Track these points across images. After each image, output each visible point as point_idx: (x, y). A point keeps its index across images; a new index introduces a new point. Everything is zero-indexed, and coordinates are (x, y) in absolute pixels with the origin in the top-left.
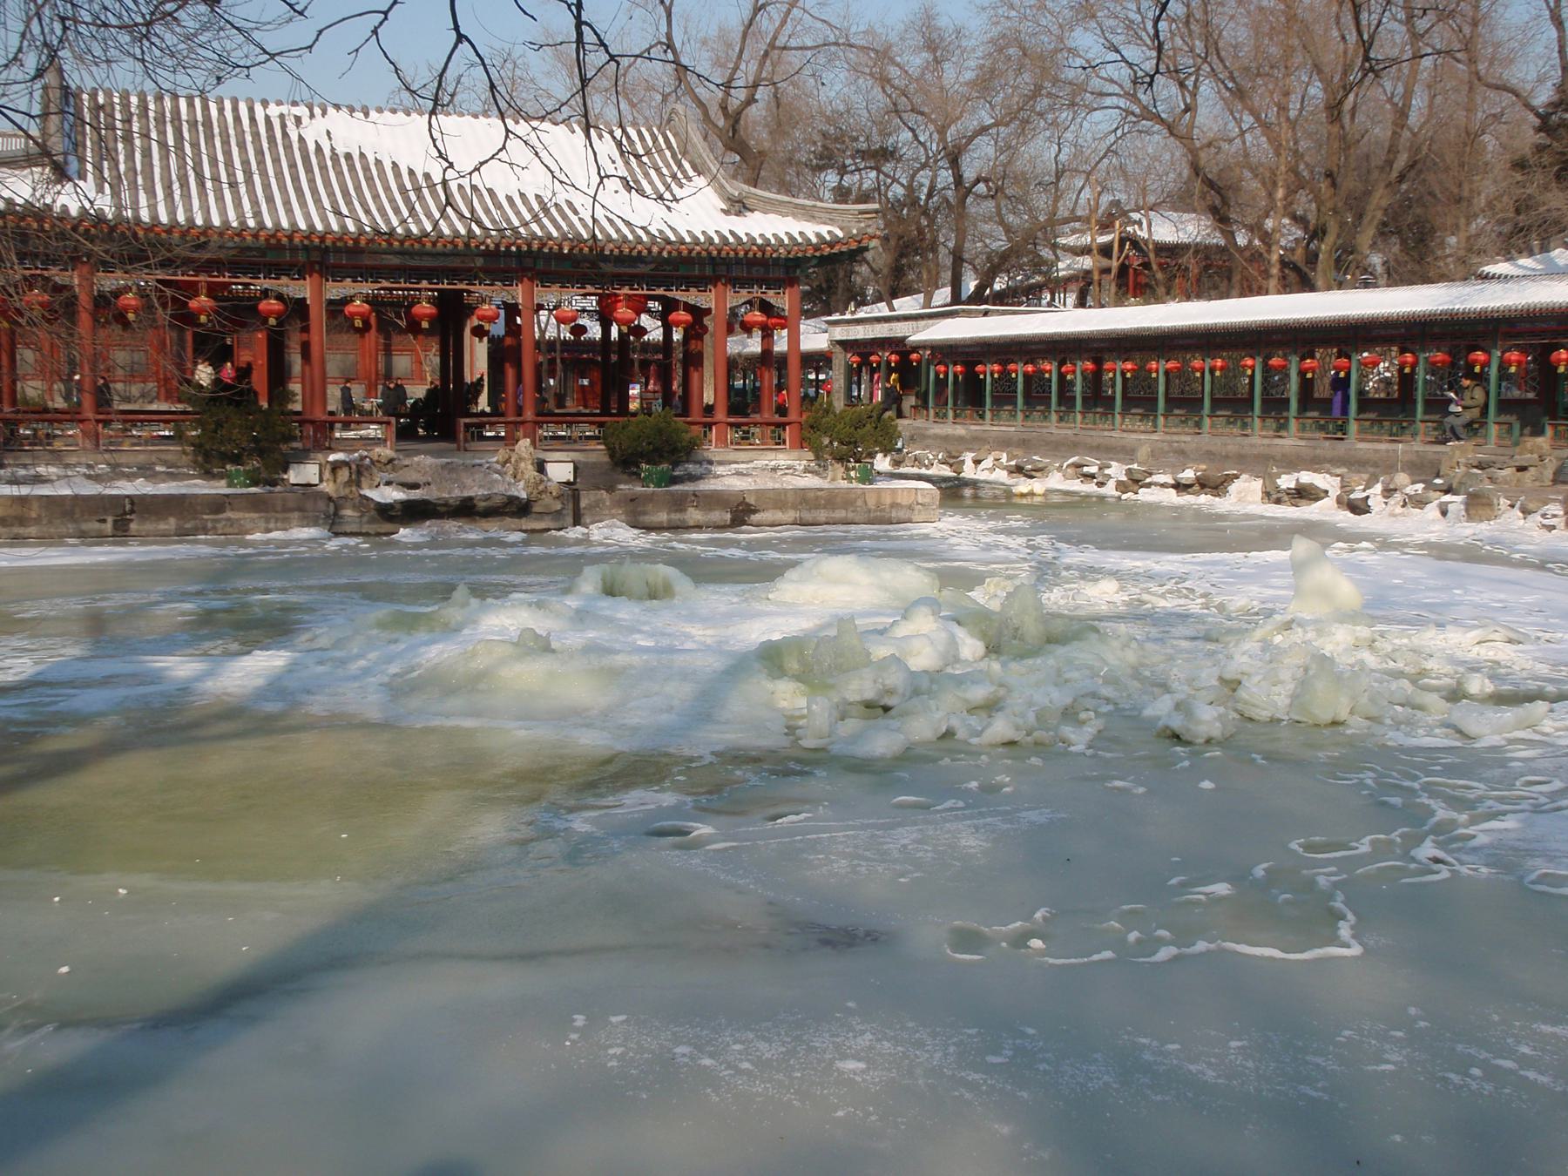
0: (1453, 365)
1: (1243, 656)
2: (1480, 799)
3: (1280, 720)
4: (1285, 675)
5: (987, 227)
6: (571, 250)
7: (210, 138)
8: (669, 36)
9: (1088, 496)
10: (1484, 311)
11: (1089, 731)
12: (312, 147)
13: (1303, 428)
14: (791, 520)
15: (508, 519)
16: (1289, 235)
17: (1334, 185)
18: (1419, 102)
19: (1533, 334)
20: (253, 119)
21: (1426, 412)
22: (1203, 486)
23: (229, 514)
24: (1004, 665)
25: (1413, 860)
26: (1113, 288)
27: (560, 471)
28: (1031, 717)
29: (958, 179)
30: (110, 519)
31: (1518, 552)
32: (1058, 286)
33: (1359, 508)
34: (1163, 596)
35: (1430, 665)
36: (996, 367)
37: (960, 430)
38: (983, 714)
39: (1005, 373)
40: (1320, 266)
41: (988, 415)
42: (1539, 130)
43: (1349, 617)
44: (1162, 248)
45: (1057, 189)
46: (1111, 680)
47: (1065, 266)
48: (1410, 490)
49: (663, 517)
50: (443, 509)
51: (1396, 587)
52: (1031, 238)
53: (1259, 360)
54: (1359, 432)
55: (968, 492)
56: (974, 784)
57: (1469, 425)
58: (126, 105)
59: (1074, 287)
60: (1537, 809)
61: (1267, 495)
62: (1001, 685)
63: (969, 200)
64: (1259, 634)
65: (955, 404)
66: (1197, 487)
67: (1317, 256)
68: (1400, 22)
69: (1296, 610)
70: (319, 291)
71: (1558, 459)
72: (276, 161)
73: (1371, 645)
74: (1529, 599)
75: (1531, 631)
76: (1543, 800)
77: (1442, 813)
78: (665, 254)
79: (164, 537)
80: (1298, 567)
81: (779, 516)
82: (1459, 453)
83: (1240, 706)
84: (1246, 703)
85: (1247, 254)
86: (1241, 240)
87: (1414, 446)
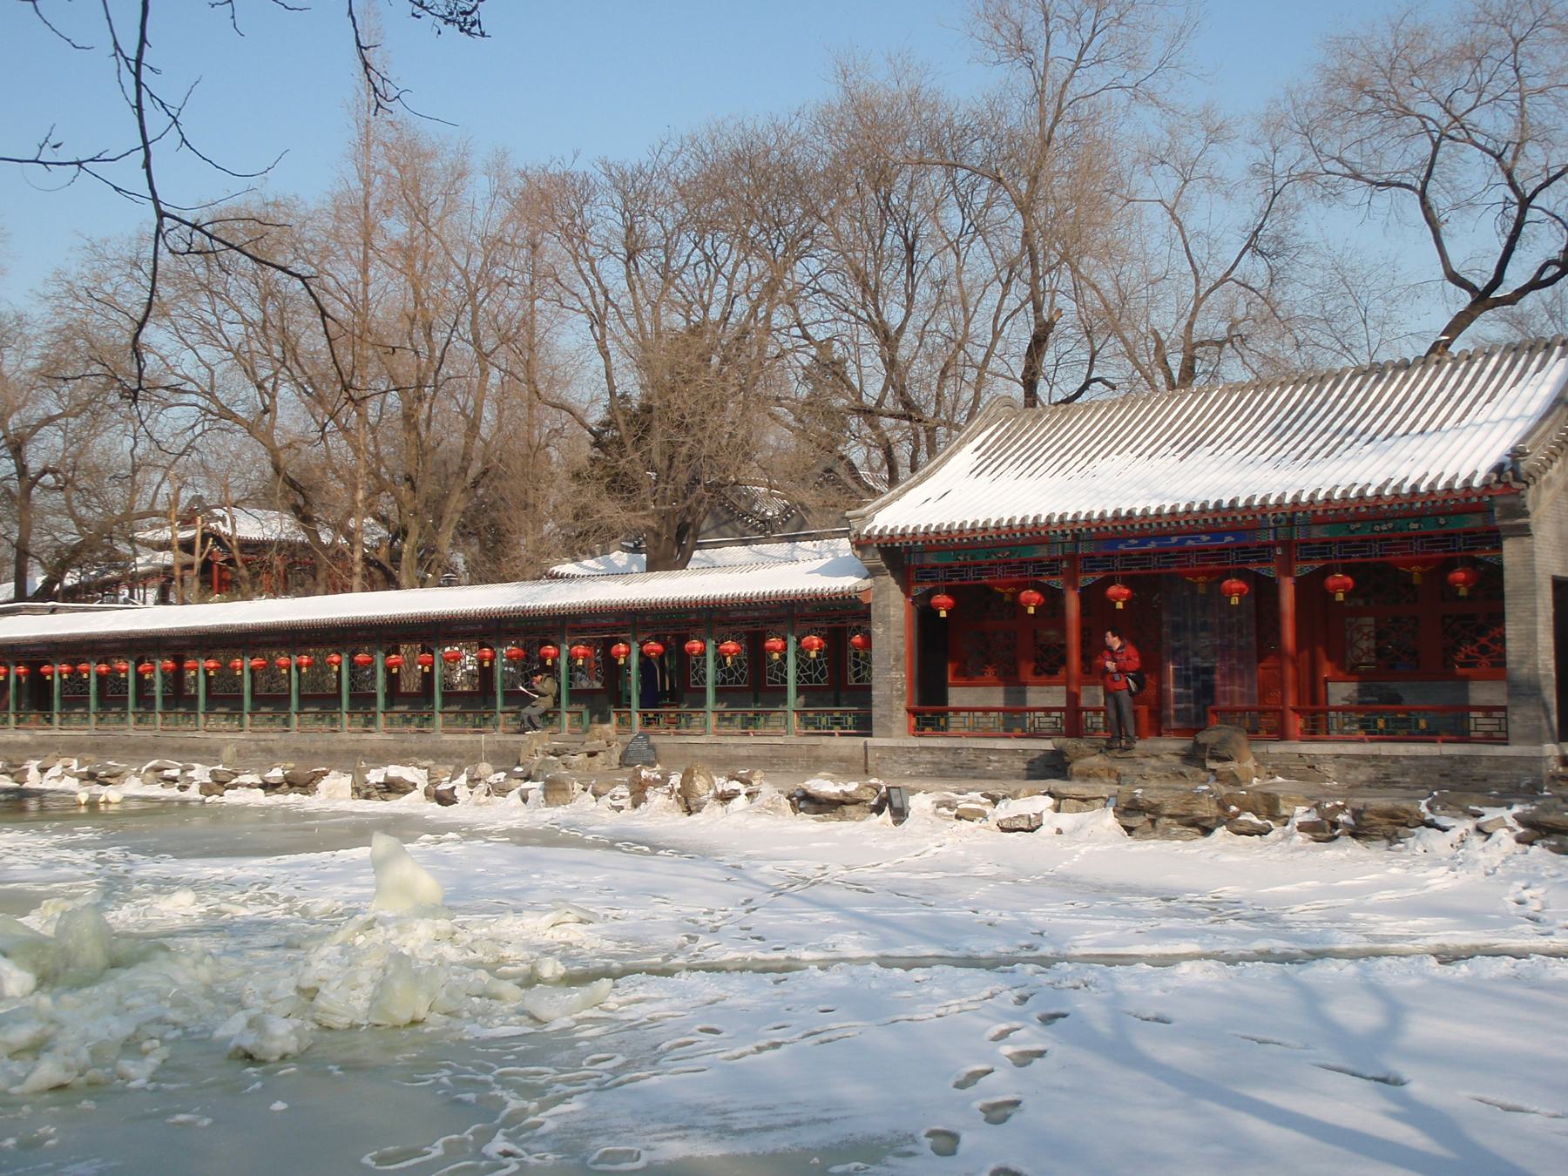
0: (527, 658)
1: (322, 962)
2: (549, 1084)
3: (358, 1026)
4: (364, 978)
5: (52, 519)
9: (169, 801)
11: (153, 1061)
13: (392, 722)
16: (372, 534)
17: (413, 488)
18: (488, 414)
19: (595, 629)
21: (505, 704)
22: (291, 785)
24: (55, 999)
25: (484, 1157)
26: (197, 585)
28: (84, 1055)
29: (22, 470)
31: (592, 833)
32: (137, 581)
33: (446, 799)
34: (243, 904)
35: (508, 952)
36: (65, 668)
37: (24, 737)
38: (28, 1057)
39: (75, 674)
40: (403, 565)
41: (57, 718)
42: (594, 445)
43: (429, 911)
44: (246, 545)
45: (133, 483)
46: (181, 1003)
47: (143, 562)
48: (493, 779)
51: (479, 876)
52: (105, 531)
53: (345, 656)
54: (444, 725)
55: (32, 804)
56: (10, 1142)
57: (544, 715)
59: (156, 582)
60: (601, 1088)
61: (356, 790)
62: (52, 1022)
63: (35, 491)
64: (340, 937)
65: (18, 708)
66: (285, 786)
67: (400, 554)
68: (467, 341)
69: (375, 908)
71: (623, 744)
73: (451, 937)
74: (599, 878)
75: (600, 910)
76: (607, 1077)
77: (514, 1103)
80: (378, 864)
82: (537, 742)
83: (318, 1016)
85: (332, 552)
86: (325, 538)
87: (495, 737)
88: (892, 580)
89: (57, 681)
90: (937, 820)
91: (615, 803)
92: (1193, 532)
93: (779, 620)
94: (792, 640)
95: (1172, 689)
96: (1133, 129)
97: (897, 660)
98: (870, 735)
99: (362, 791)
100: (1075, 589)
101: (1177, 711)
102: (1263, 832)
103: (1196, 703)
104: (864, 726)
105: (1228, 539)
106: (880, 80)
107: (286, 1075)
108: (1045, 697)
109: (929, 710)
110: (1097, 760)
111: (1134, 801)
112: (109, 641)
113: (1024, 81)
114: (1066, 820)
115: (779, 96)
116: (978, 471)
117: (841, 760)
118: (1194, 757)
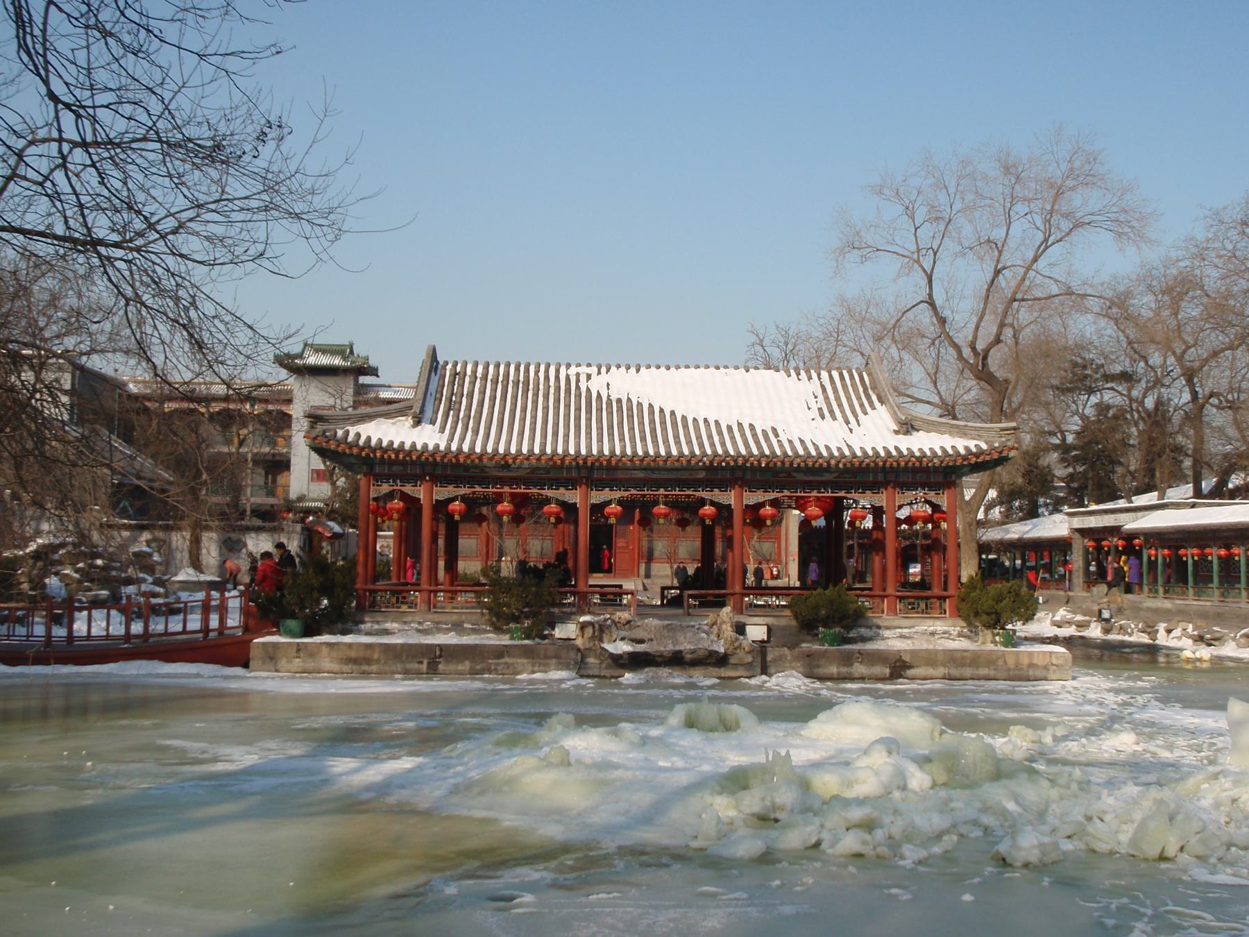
6: (767, 464)
7: (526, 391)
8: (930, 295)
12: (594, 396)
14: (941, 675)
15: (711, 669)
20: (557, 378)
23: (506, 660)
27: (756, 632)
29: (1195, 394)
30: (425, 662)
36: (1195, 551)
37: (1167, 604)
39: (1203, 557)
49: (834, 670)
50: (659, 659)
58: (474, 372)
70: (586, 498)
72: (568, 406)
78: (841, 465)
79: (460, 675)
81: (930, 671)
84: (1094, 837)
89: (1190, 562)
107: (1010, 878)
112: (1224, 531)
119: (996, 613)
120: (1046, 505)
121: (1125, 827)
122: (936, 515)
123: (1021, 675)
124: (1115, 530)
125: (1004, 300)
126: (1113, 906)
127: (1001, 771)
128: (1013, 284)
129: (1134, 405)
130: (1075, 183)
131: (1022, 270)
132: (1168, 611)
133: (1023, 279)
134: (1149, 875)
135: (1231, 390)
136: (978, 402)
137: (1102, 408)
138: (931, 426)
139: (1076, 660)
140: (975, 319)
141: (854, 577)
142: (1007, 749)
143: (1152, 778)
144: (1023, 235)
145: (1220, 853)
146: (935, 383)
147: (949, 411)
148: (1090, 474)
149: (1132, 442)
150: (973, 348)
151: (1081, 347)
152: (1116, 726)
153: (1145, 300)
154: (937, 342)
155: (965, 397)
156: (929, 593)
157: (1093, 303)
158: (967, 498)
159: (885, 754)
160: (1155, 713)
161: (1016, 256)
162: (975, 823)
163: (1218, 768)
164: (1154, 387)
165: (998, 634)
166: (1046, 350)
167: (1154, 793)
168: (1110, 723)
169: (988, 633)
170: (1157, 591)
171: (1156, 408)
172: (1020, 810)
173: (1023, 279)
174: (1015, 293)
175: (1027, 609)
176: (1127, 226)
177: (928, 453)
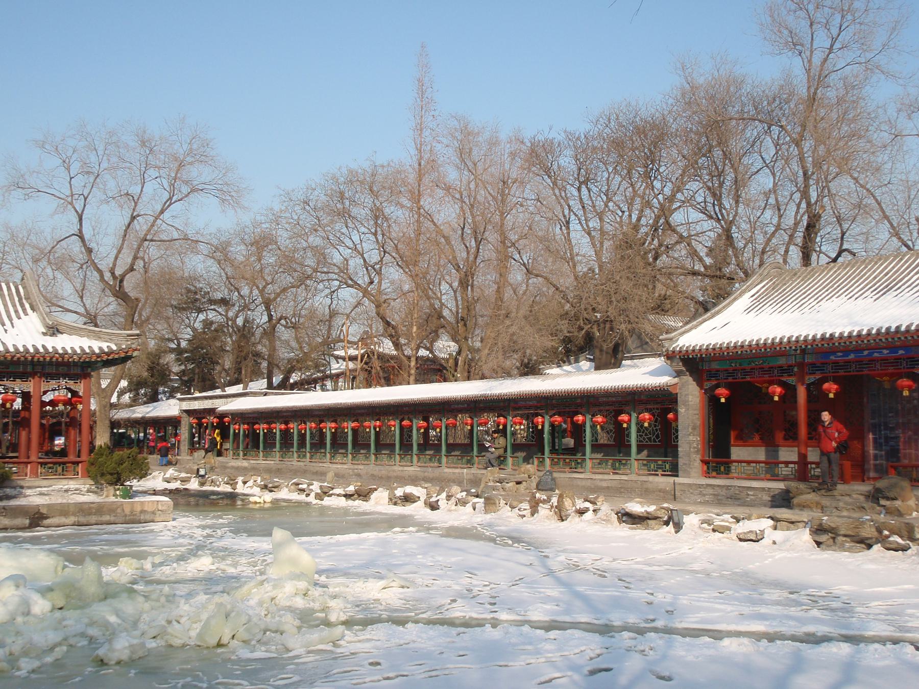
8: (80, 230)
10: (500, 395)
14: (71, 523)
29: (270, 317)
33: (434, 507)
36: (265, 426)
37: (245, 464)
39: (270, 430)
47: (336, 367)
48: (459, 496)
53: (634, 415)
66: (356, 496)
81: (63, 520)
88: (690, 379)
89: (262, 433)
90: (701, 532)
91: (521, 513)
92: (877, 348)
93: (626, 403)
94: (634, 415)
95: (871, 451)
96: (880, 94)
97: (694, 428)
98: (677, 476)
99: (393, 501)
100: (803, 385)
101: (875, 465)
102: (904, 549)
103: (887, 460)
104: (674, 471)
105: (901, 352)
106: (704, 74)
107: (104, 674)
108: (788, 454)
109: (718, 459)
110: (812, 497)
111: (821, 525)
113: (797, 67)
114: (779, 535)
115: (650, 89)
116: (748, 310)
117: (660, 491)
118: (875, 497)
119: (118, 473)
120: (164, 392)
121: (195, 626)
122: (74, 399)
123: (134, 520)
124: (211, 411)
125: (138, 239)
126: (179, 685)
127: (109, 593)
128: (145, 228)
129: (230, 323)
130: (193, 159)
131: (152, 219)
132: (245, 468)
133: (153, 225)
134: (211, 659)
135: (294, 315)
136: (115, 314)
137: (207, 323)
138: (73, 330)
139: (176, 506)
140: (115, 252)
141: (8, 448)
142: (116, 576)
143: (220, 588)
144: (153, 192)
145: (258, 637)
146: (82, 297)
147: (92, 319)
148: (197, 371)
149: (228, 348)
150: (113, 274)
151: (194, 278)
152: (200, 553)
153: (239, 248)
154: (84, 266)
155: (106, 310)
156: (66, 459)
157: (201, 247)
158: (103, 386)
159: (13, 588)
160: (230, 541)
161: (148, 207)
162: (83, 635)
163: (264, 577)
164: (243, 310)
165: (118, 489)
166: (168, 279)
167: (217, 599)
168: (196, 551)
169: (111, 488)
170: (238, 455)
171: (244, 326)
172: (119, 621)
173: (153, 225)
174: (146, 235)
175: (142, 470)
176: (228, 195)
177: (70, 351)
